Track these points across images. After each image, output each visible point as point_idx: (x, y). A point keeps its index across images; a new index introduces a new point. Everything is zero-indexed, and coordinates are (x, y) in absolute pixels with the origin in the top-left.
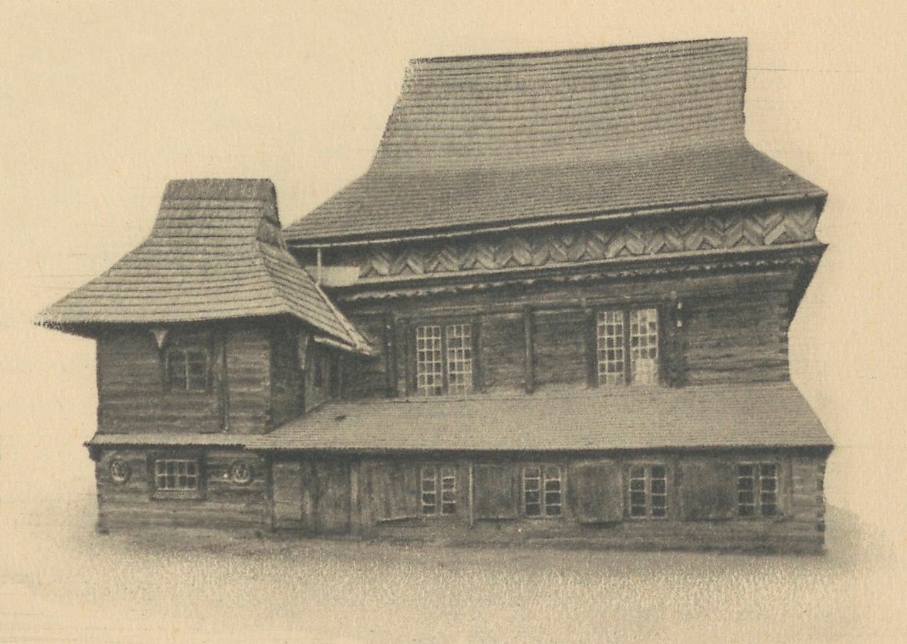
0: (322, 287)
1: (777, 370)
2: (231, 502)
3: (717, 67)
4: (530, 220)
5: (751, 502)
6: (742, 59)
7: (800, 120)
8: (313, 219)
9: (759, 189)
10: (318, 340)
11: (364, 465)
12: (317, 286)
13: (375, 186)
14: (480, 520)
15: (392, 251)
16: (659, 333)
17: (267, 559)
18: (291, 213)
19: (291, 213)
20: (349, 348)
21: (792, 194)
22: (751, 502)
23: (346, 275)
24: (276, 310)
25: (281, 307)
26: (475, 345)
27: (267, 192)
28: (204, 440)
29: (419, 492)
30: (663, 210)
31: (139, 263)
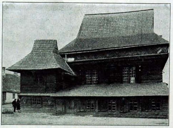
0: (67, 63)
1: (160, 80)
2: (48, 108)
3: (147, 16)
4: (113, 48)
5: (156, 106)
6: (152, 15)
7: (167, 30)
8: (67, 47)
9: (156, 43)
10: (65, 73)
11: (75, 99)
12: (65, 62)
13: (79, 41)
14: (99, 111)
15: (73, 56)
16: (123, 80)
17: (112, 86)
18: (60, 47)
19: (60, 47)
20: (72, 75)
21: (162, 43)
22: (156, 106)
23: (72, 60)
24: (57, 67)
25: (58, 66)
26: (27, 101)
27: (55, 43)
28: (42, 95)
29: (86, 105)
30: (130, 47)
31: (30, 58)
